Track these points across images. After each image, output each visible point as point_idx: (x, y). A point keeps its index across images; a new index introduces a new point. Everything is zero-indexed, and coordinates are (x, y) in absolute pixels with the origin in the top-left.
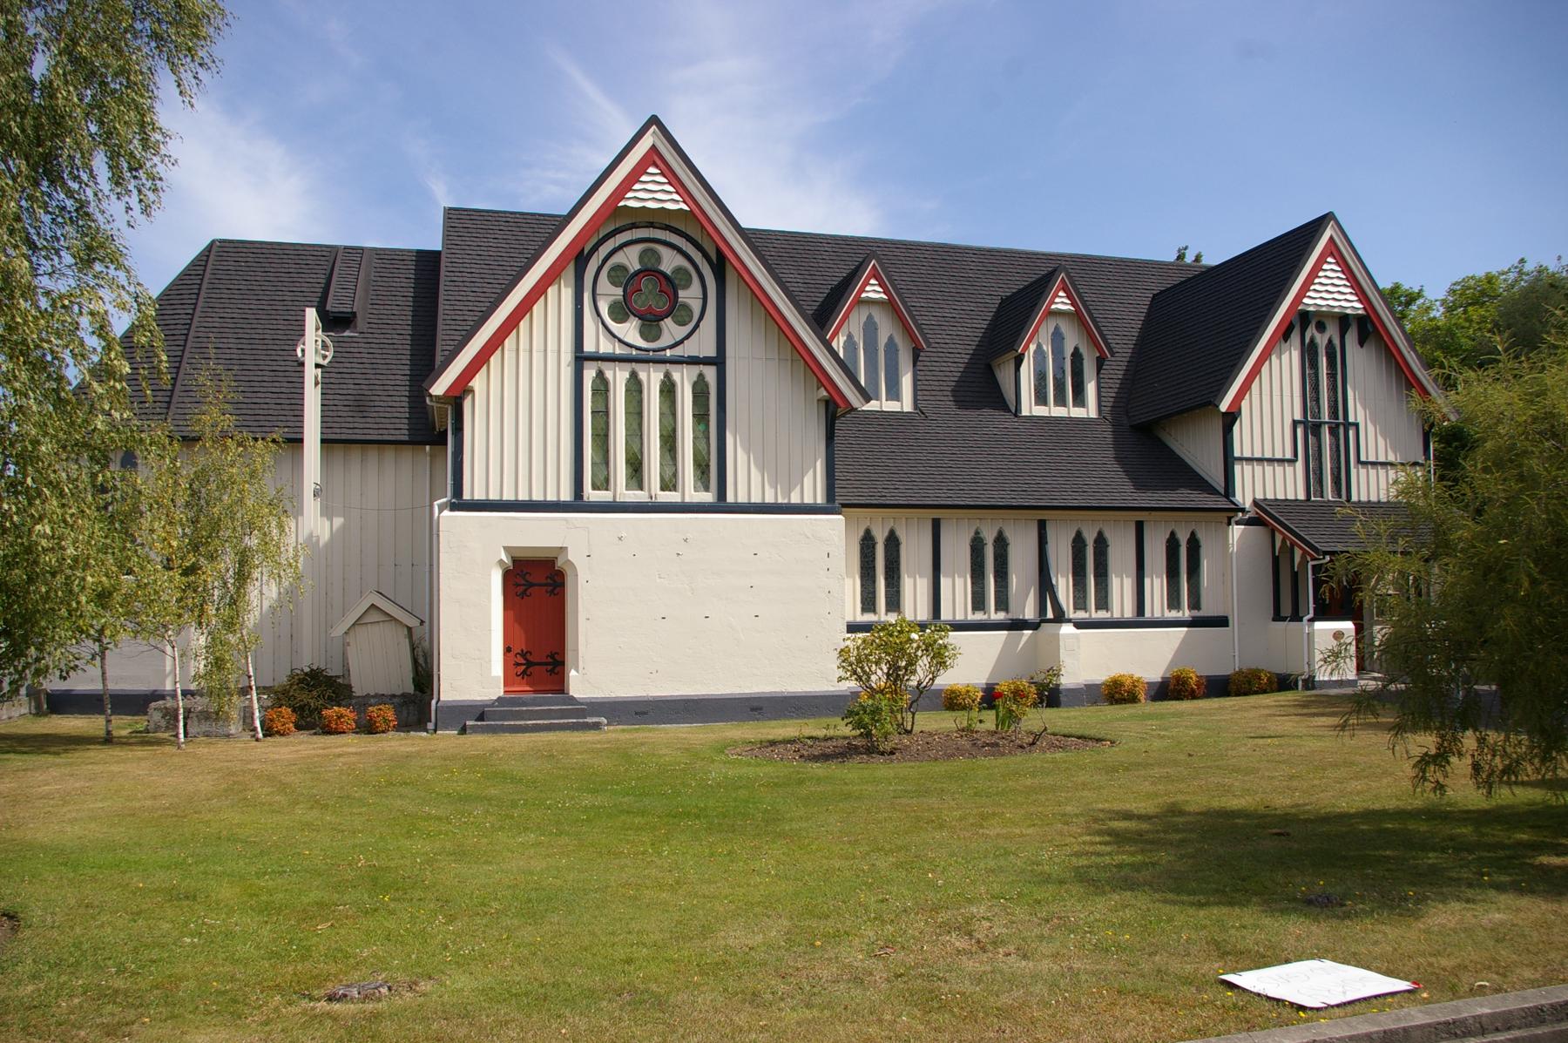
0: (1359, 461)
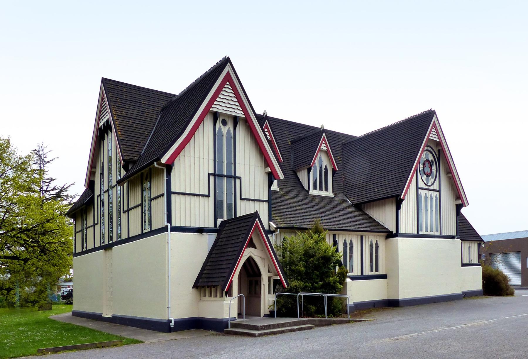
0: (241, 199)
